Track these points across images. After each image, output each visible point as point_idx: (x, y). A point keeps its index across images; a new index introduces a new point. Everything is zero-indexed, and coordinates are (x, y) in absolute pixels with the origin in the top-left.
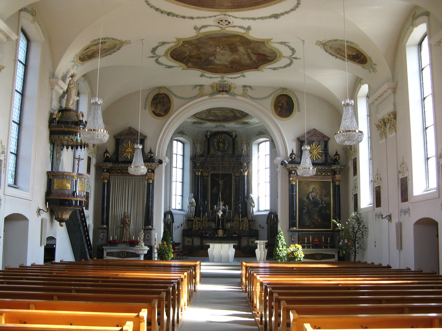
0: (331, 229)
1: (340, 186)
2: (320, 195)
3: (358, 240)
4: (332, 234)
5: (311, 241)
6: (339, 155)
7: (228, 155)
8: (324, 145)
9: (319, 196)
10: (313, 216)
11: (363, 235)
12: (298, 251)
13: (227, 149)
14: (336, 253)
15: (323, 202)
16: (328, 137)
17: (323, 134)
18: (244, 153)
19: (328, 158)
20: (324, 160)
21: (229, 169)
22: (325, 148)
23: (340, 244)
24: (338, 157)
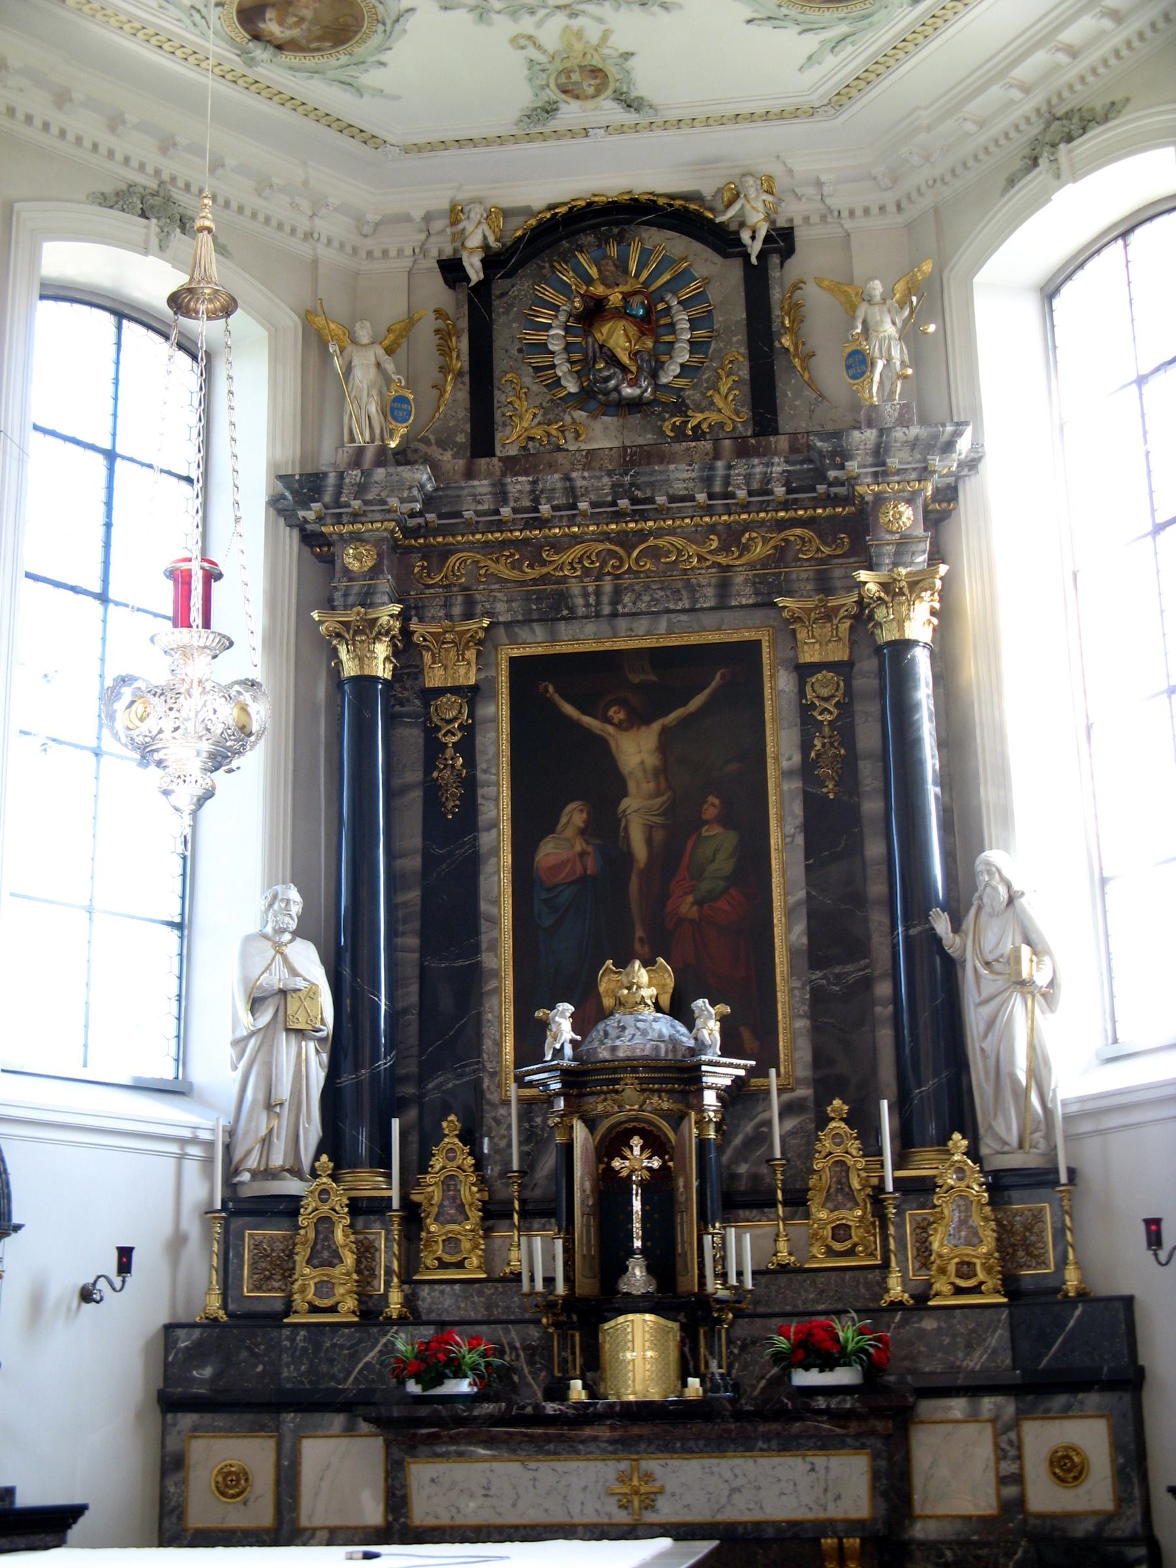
13: (682, 382)
21: (724, 587)
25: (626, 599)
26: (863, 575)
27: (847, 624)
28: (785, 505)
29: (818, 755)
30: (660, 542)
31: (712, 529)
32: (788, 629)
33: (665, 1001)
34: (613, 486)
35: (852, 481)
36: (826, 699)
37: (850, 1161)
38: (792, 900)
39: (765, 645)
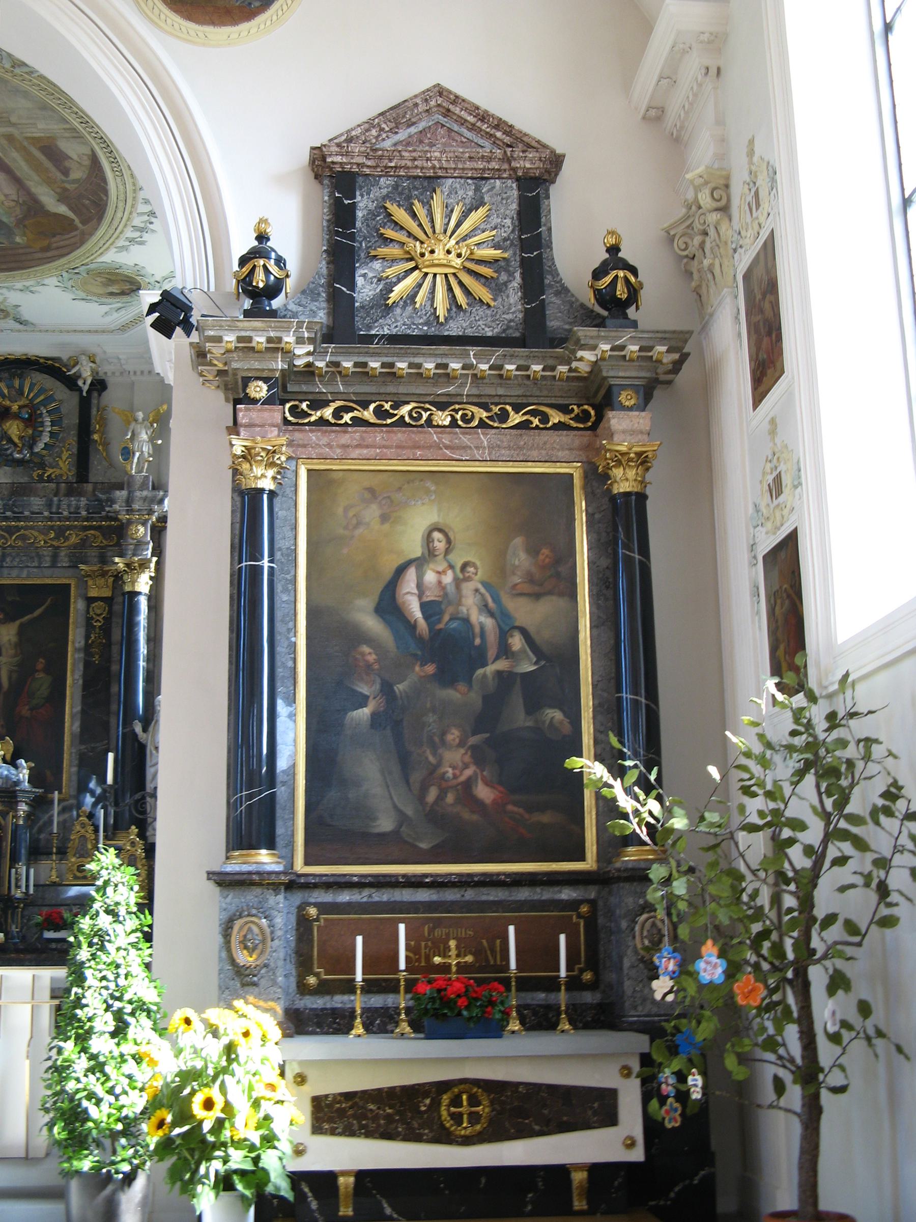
0: (589, 864)
1: (649, 503)
2: (484, 584)
3: (841, 955)
4: (592, 903)
5: (402, 965)
6: (634, 271)
7: (53, 486)
8: (514, 206)
9: (483, 590)
10: (431, 759)
11: (883, 890)
12: (225, 1070)
13: (44, 452)
14: (626, 1072)
15: (517, 642)
16: (545, 146)
17: (505, 123)
18: (139, 471)
19: (549, 297)
20: (520, 316)
21: (55, 558)
22: (522, 232)
23: (658, 996)
24: (626, 280)
25: (8, 560)
26: (117, 560)
27: (112, 579)
28: (87, 519)
29: (93, 642)
30: (26, 532)
31: (52, 528)
32: (83, 581)
33: (8, 757)
34: (4, 505)
35: (117, 512)
36: (99, 615)
37: (88, 836)
38: (75, 710)
39: (73, 586)
